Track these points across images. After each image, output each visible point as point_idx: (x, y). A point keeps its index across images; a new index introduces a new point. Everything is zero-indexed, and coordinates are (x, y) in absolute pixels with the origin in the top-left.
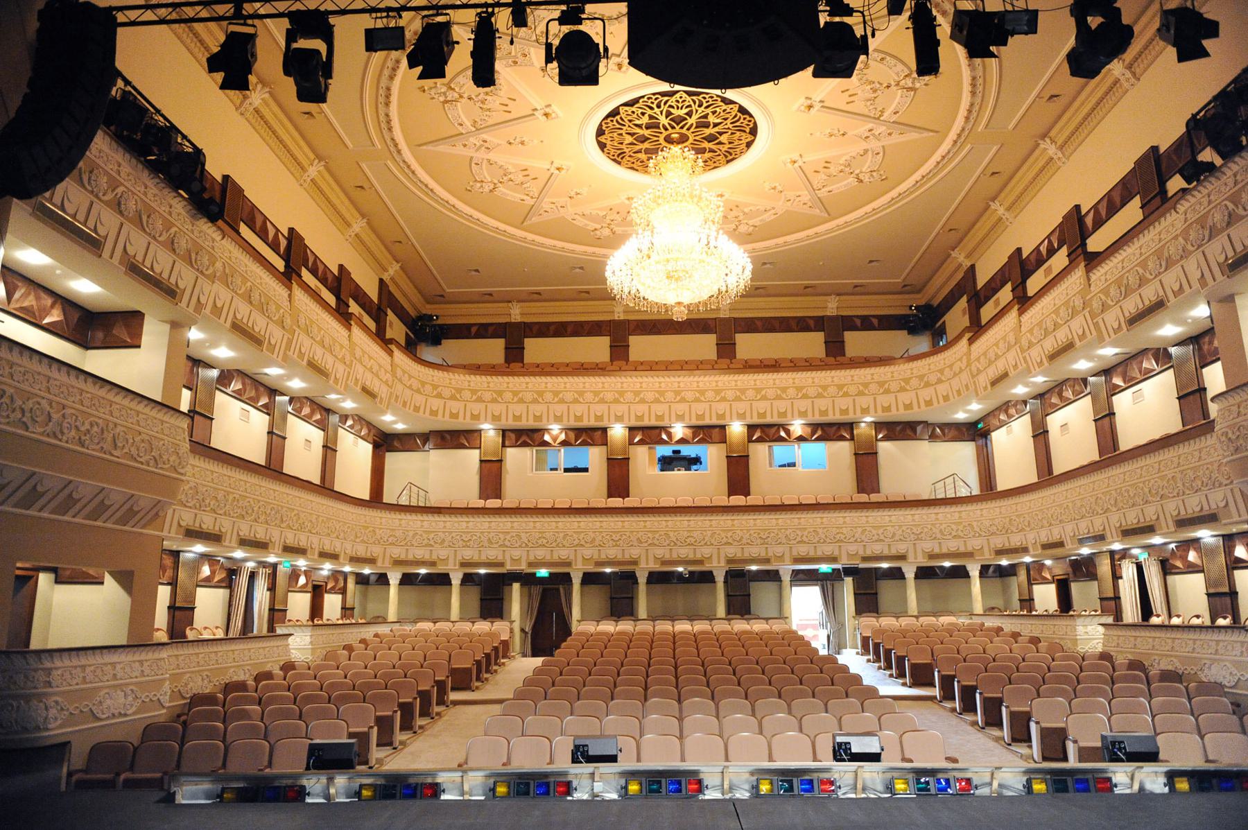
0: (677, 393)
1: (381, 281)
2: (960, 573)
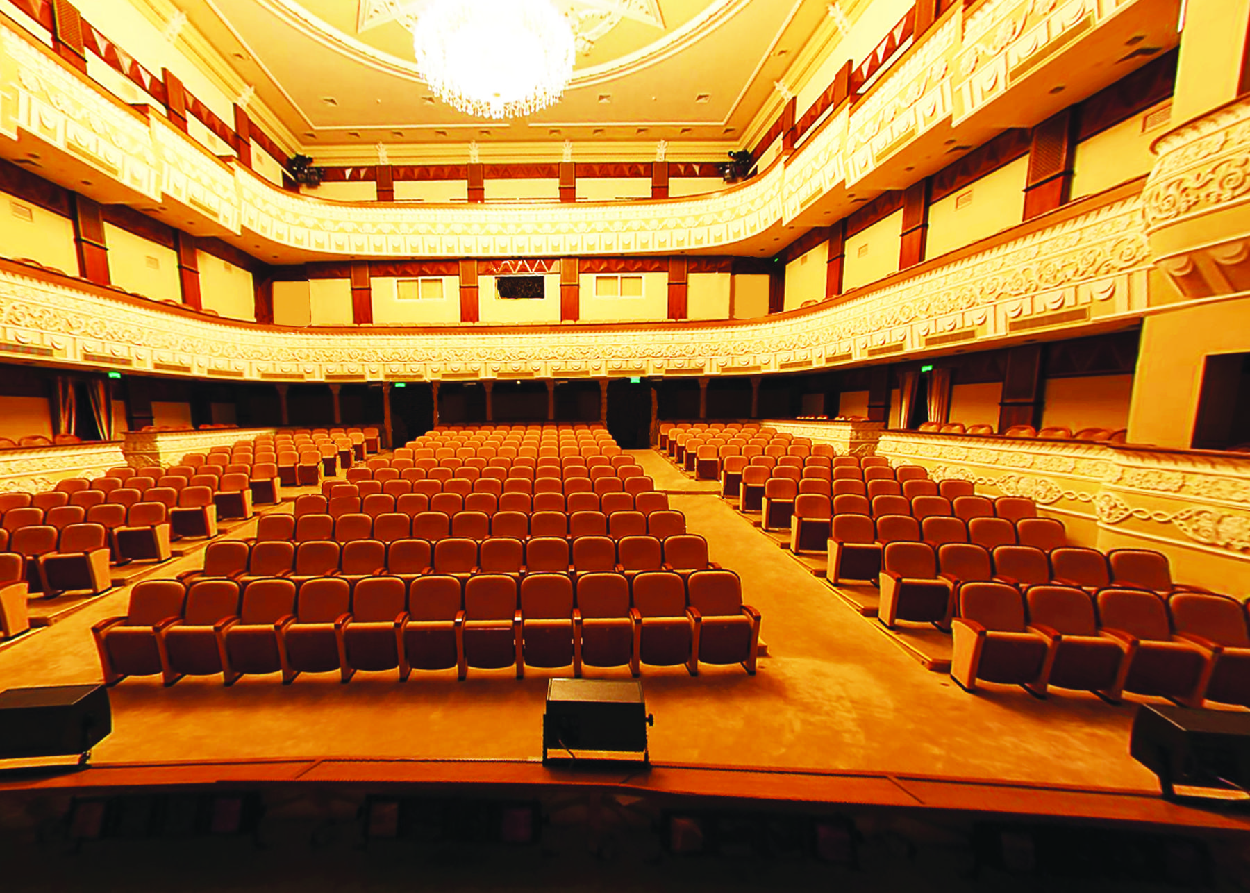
1: (235, 105)
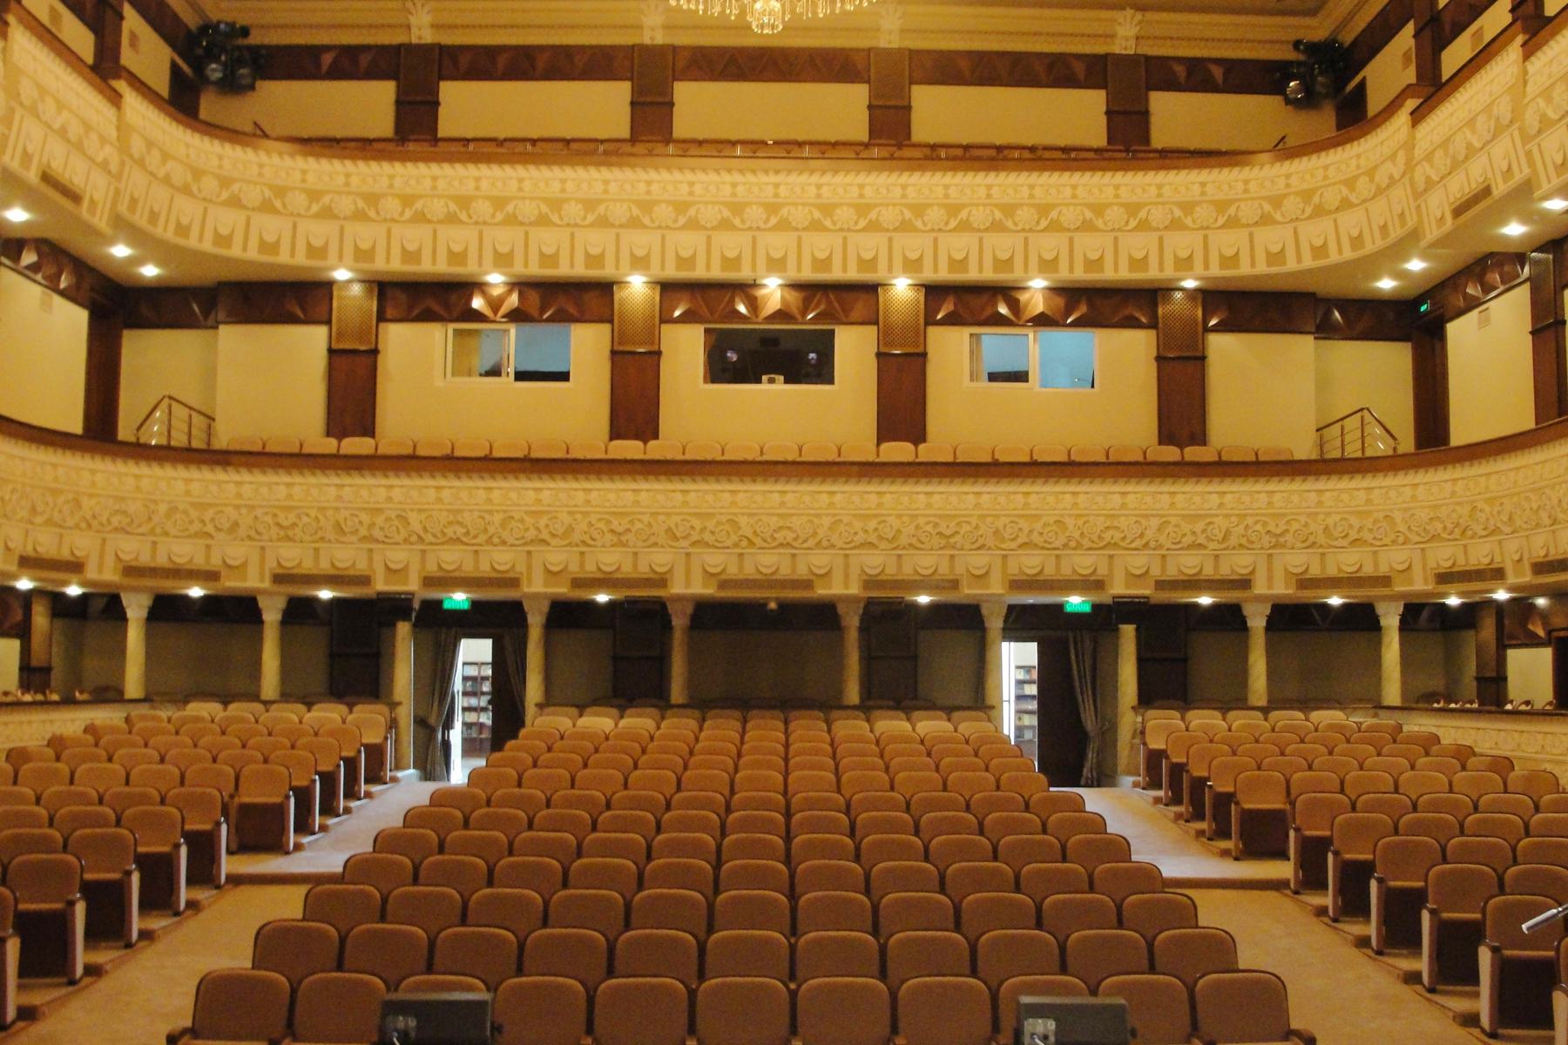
0: (772, 208)
2: (1361, 618)
